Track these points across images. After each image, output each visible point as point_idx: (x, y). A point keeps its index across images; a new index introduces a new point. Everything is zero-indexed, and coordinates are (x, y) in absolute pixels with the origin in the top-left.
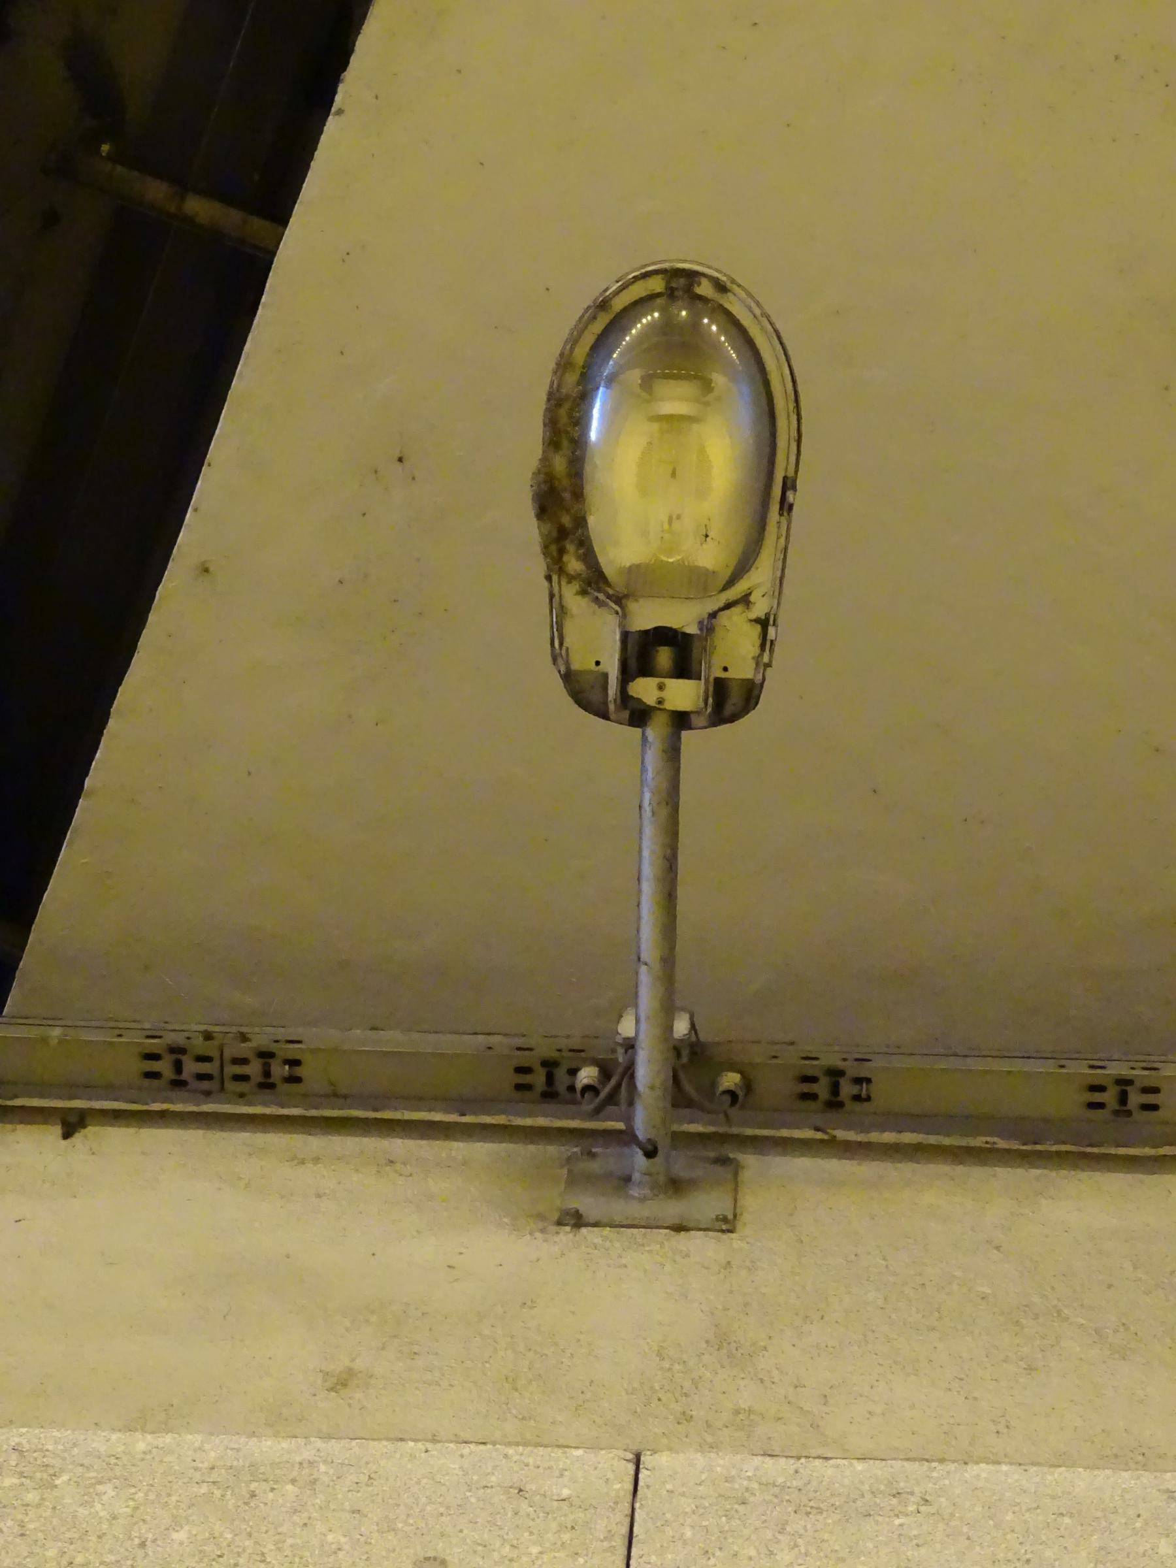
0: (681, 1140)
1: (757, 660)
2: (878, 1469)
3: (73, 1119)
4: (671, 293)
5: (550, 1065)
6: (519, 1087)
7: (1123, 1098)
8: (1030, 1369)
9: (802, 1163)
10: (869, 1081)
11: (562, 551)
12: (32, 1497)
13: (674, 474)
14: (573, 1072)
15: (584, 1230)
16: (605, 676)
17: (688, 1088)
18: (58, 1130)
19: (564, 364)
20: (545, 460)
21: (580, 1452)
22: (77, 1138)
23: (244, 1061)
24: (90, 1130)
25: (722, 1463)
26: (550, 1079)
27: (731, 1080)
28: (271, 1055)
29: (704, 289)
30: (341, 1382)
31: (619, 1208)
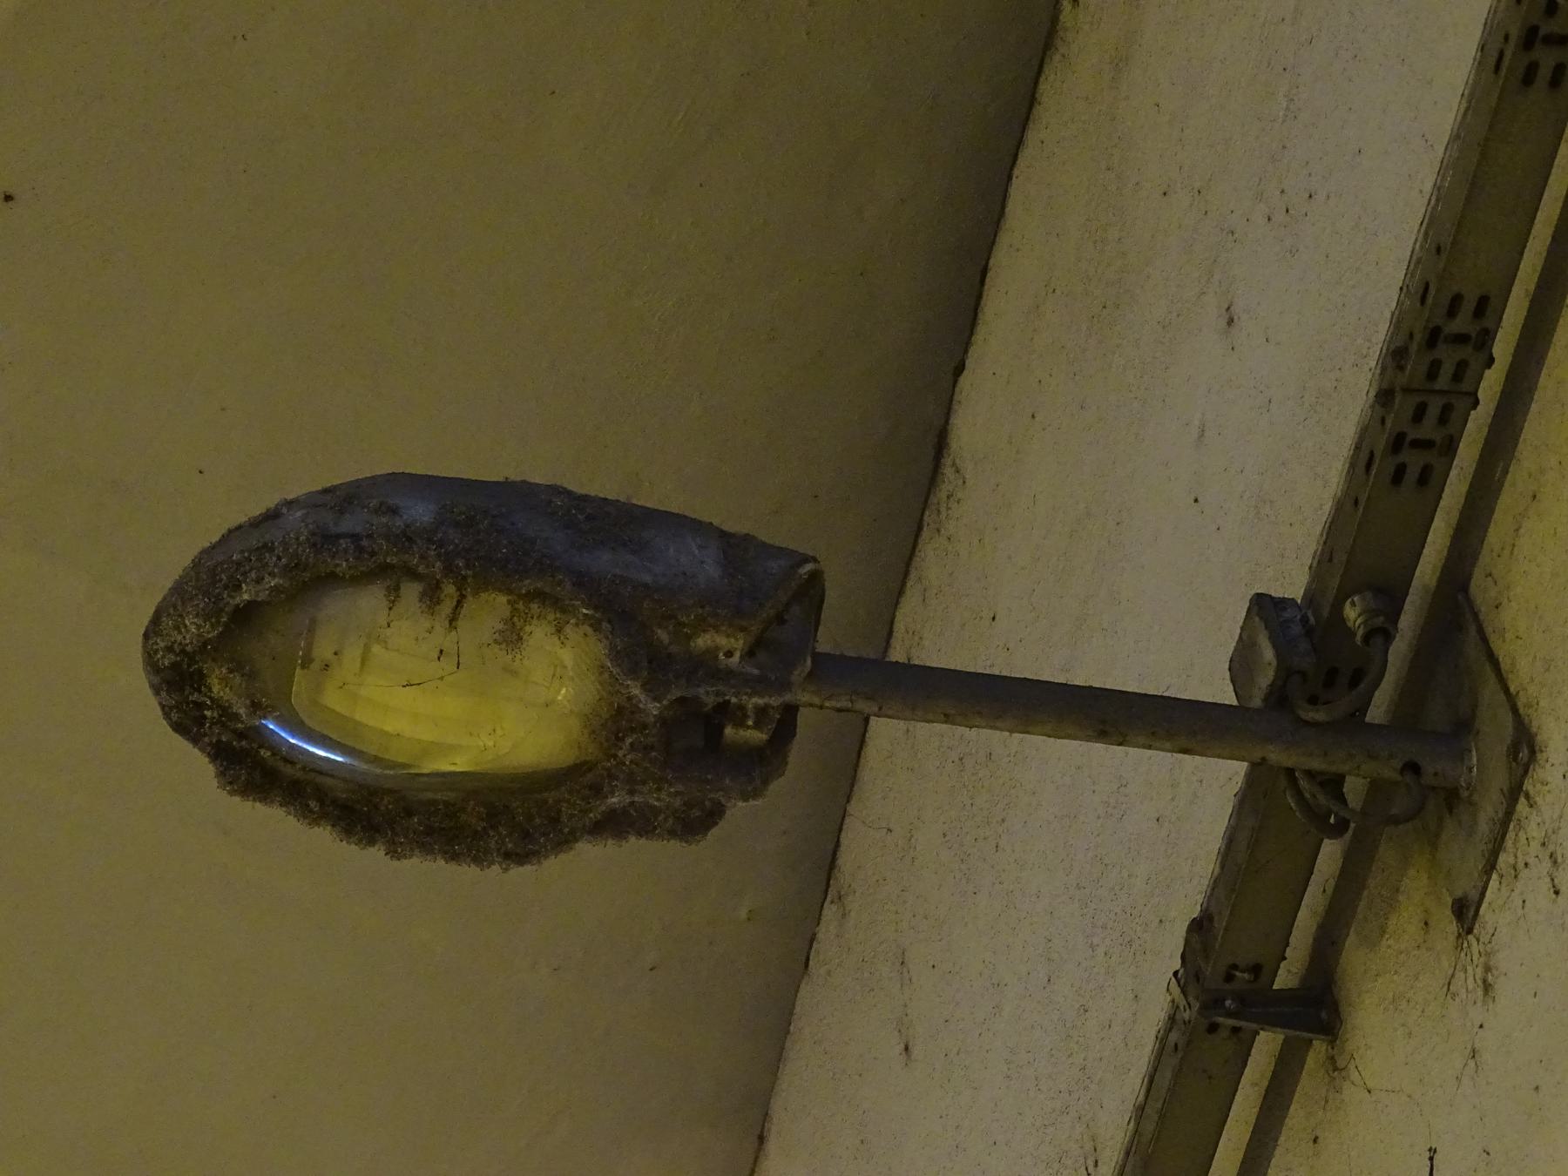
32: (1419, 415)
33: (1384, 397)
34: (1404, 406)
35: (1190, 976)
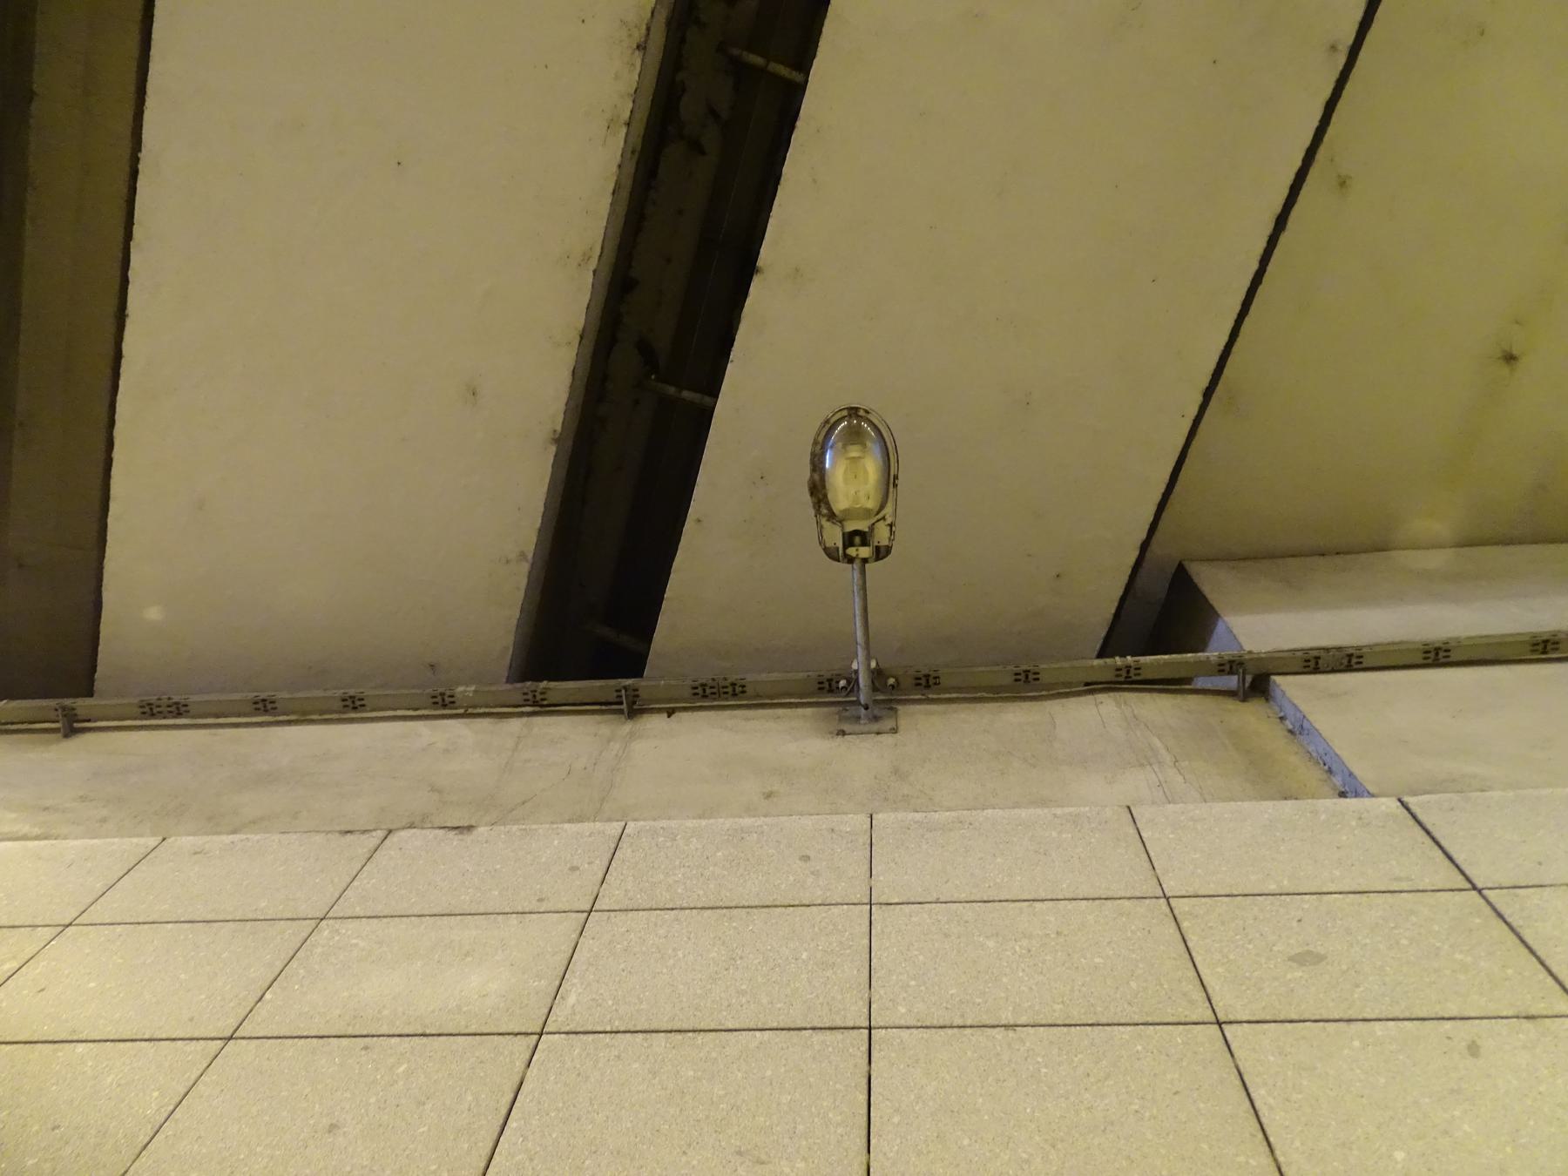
0: (876, 702)
1: (890, 539)
2: (954, 814)
3: (671, 711)
4: (850, 416)
5: (830, 680)
6: (820, 689)
7: (1027, 677)
8: (1002, 774)
9: (918, 707)
10: (939, 677)
11: (820, 507)
12: (669, 844)
13: (856, 477)
14: (838, 682)
15: (846, 737)
16: (838, 549)
17: (877, 684)
18: (666, 715)
19: (815, 443)
20: (811, 476)
21: (851, 815)
22: (673, 717)
23: (726, 687)
24: (677, 714)
25: (900, 815)
26: (830, 685)
27: (891, 681)
28: (735, 684)
29: (861, 413)
30: (769, 796)
31: (857, 728)
32: (711, 687)
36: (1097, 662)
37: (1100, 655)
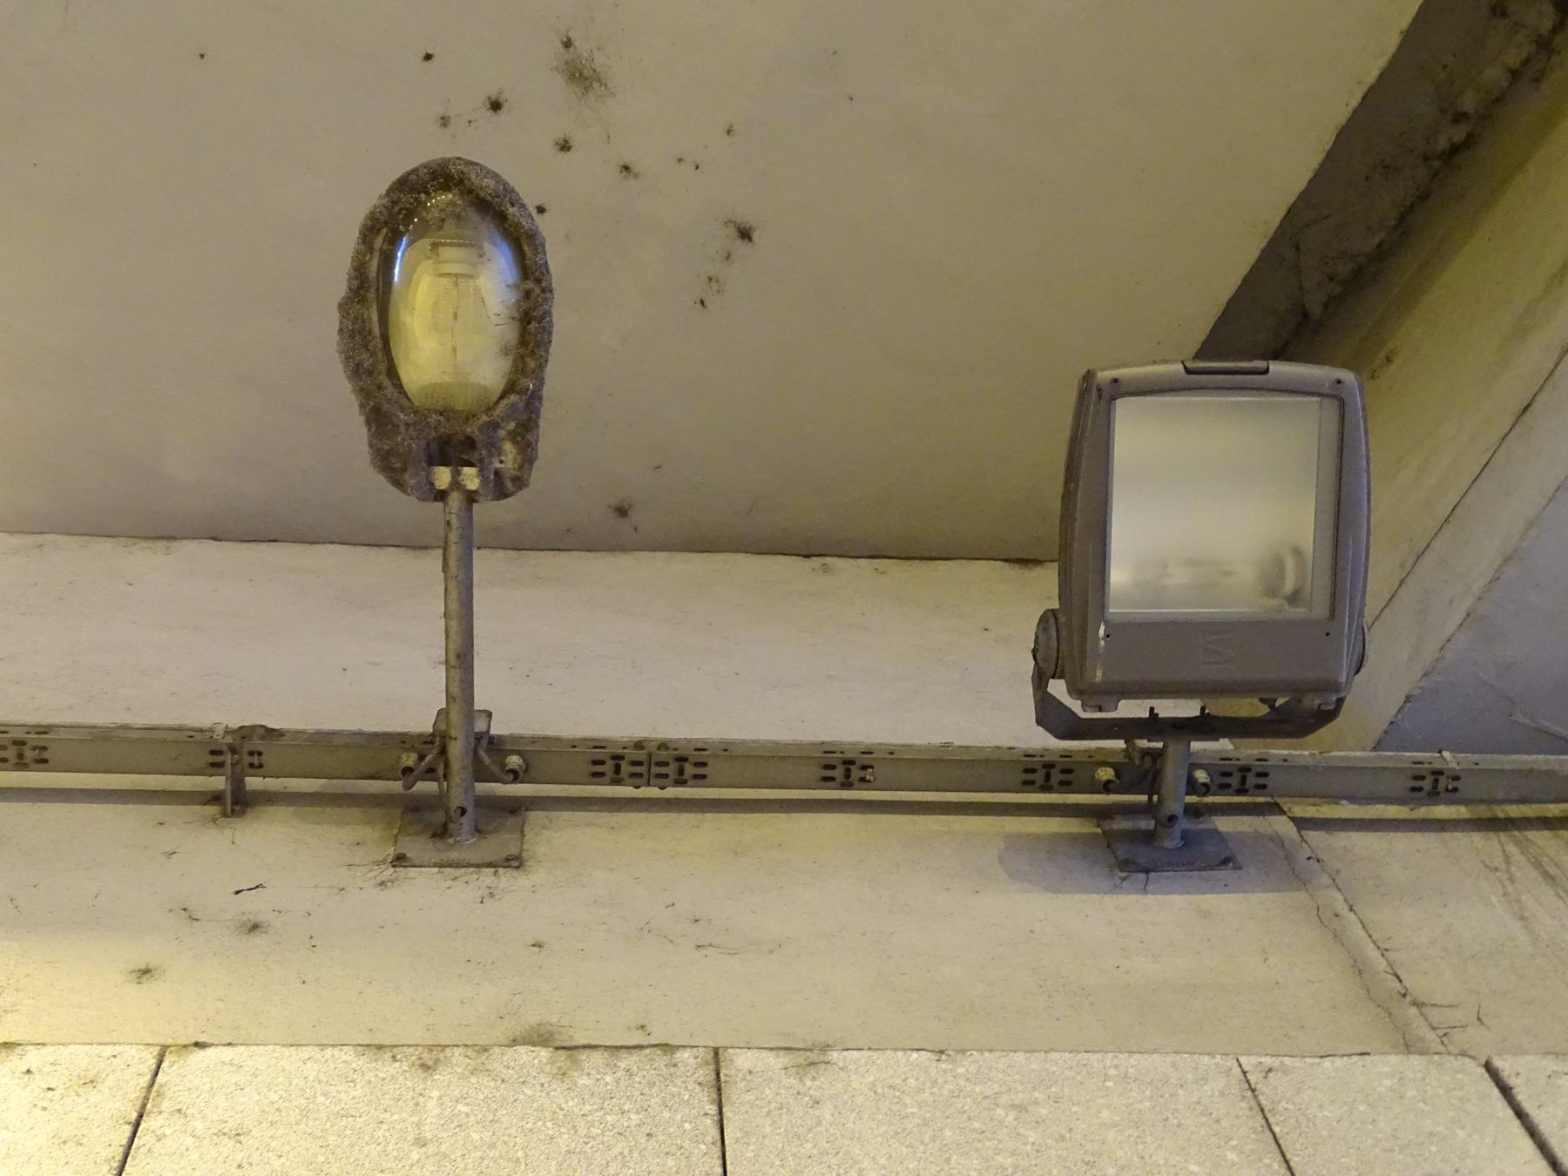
23: (666, 764)
32: (635, 763)
33: (639, 745)
34: (640, 755)
35: (245, 733)
36: (1372, 754)
37: (1374, 749)
